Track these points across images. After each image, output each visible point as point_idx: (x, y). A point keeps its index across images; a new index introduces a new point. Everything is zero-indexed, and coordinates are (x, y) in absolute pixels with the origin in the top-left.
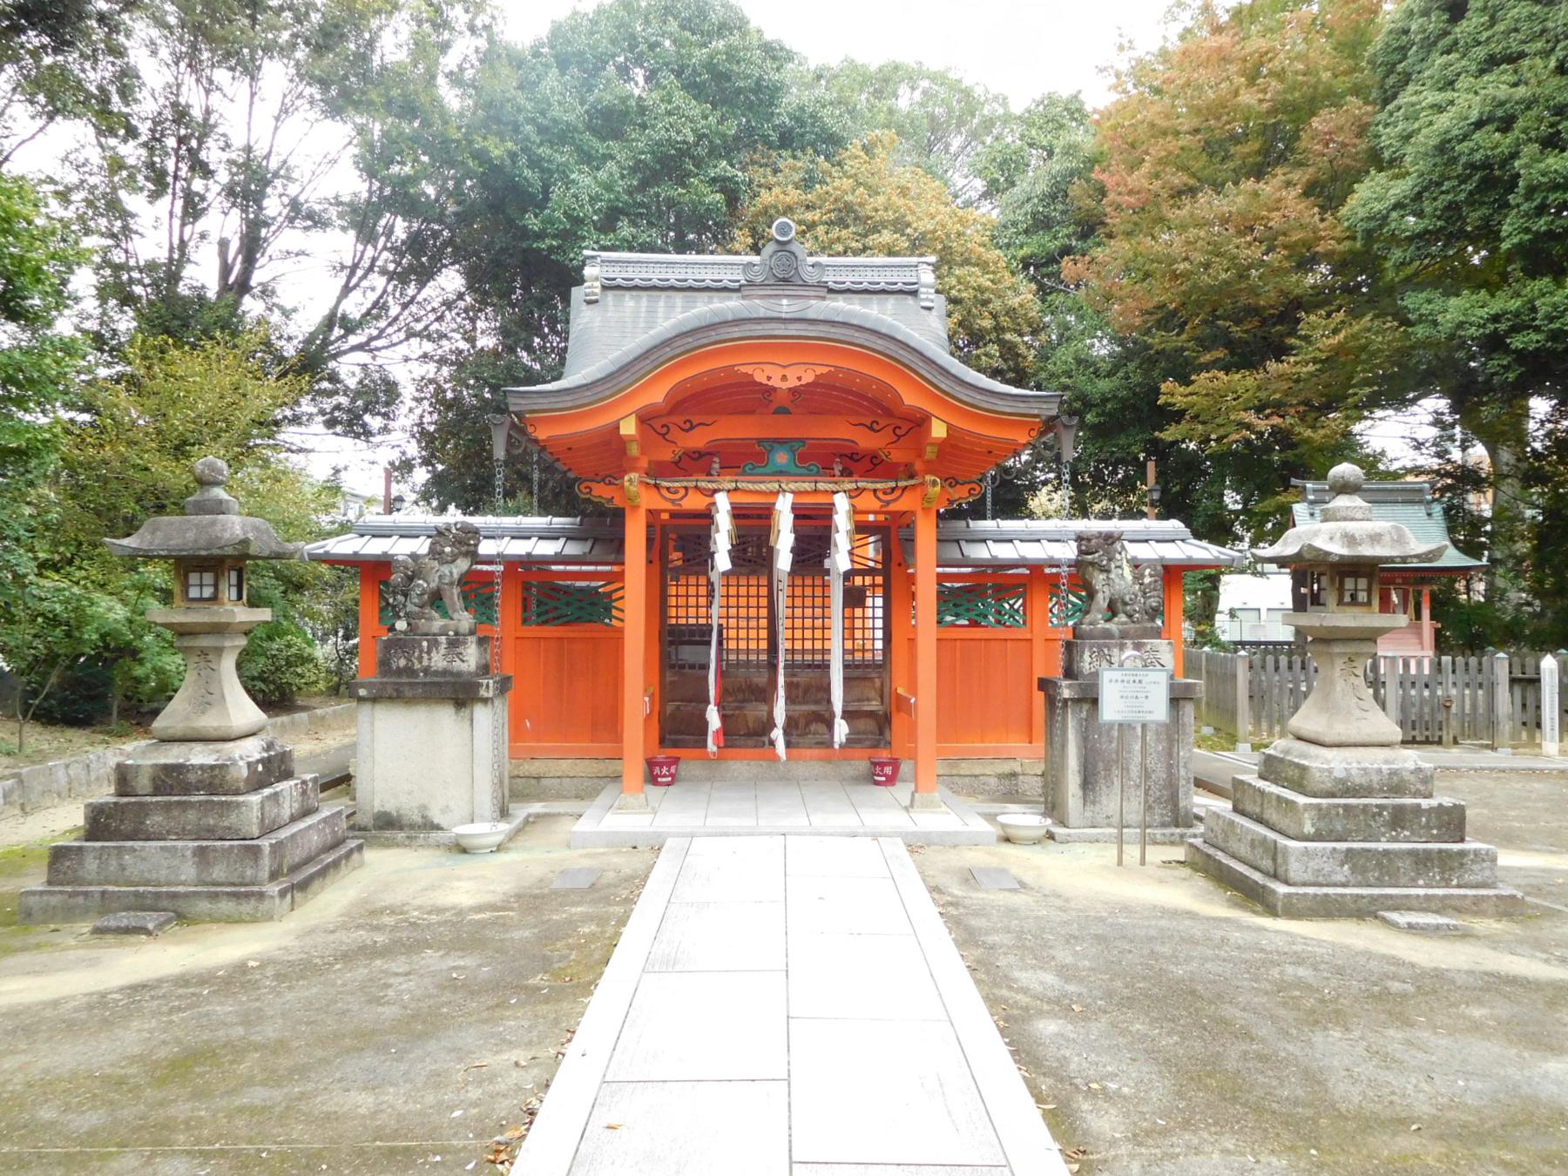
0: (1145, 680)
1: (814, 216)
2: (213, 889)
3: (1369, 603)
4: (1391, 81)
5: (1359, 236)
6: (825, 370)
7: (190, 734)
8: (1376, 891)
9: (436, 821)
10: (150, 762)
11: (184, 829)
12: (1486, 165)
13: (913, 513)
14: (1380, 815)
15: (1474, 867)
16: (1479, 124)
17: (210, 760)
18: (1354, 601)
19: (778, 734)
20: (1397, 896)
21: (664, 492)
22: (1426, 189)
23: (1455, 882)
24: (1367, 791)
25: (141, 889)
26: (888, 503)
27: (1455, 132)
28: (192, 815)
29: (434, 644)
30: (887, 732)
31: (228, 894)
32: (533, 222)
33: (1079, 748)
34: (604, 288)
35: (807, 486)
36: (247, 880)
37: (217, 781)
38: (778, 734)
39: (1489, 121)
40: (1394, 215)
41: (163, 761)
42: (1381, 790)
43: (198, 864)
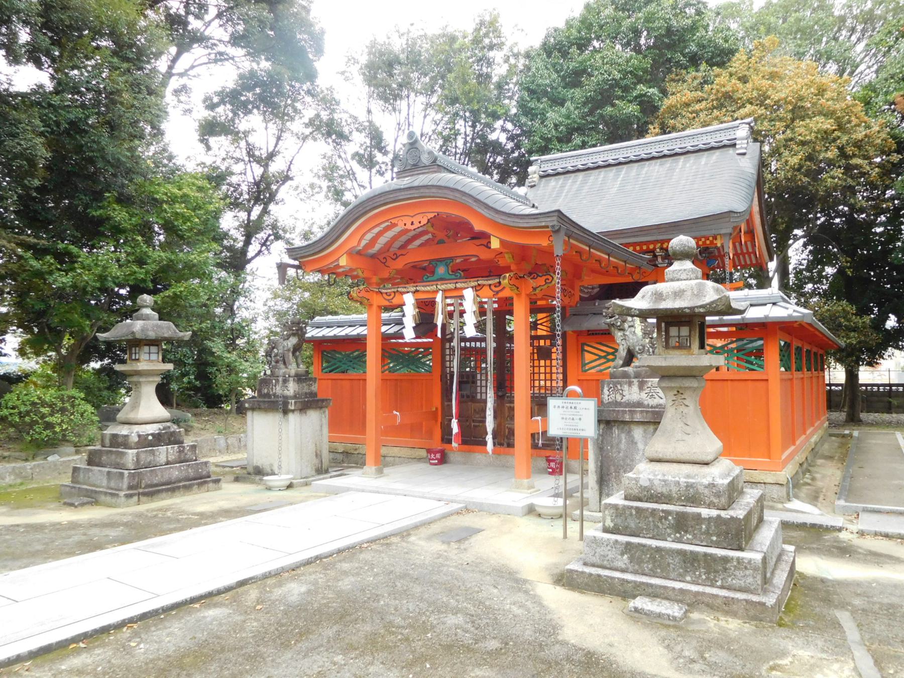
0: (578, 406)
2: (94, 488)
6: (432, 215)
8: (644, 579)
13: (512, 299)
14: (666, 519)
15: (737, 573)
18: (680, 347)
19: (489, 438)
20: (657, 586)
21: (385, 295)
23: (719, 583)
24: (666, 498)
26: (497, 292)
33: (596, 455)
38: (489, 438)
42: (679, 499)
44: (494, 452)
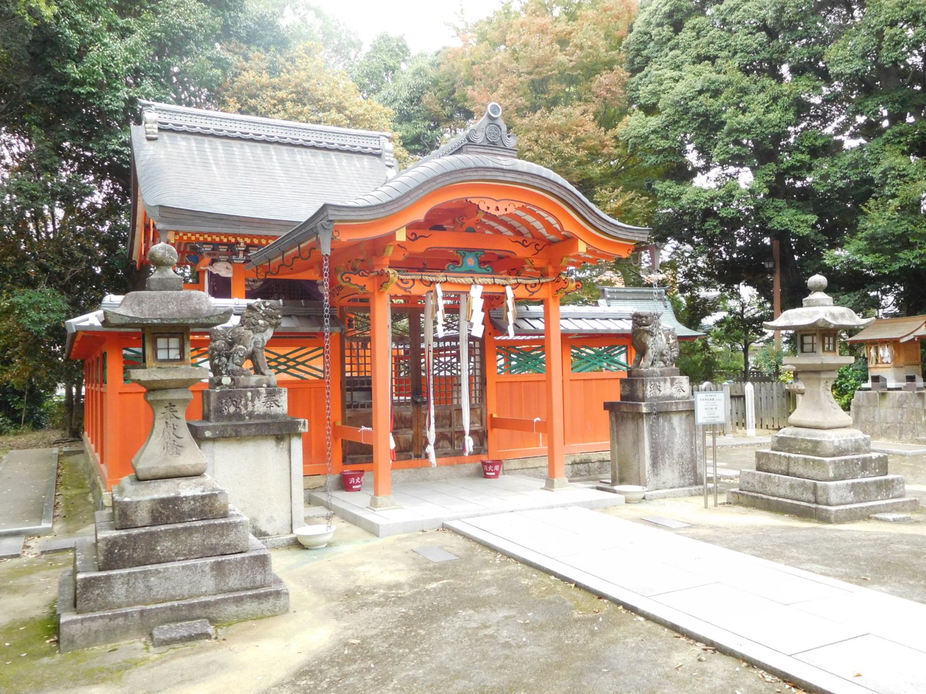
1: (282, 94)
3: (834, 350)
4: (638, 59)
5: (630, 146)
7: (171, 472)
9: (263, 530)
10: (148, 498)
11: (190, 550)
12: (705, 115)
16: (700, 92)
17: (198, 492)
19: (430, 449)
22: (670, 124)
25: (176, 603)
26: (533, 293)
27: (688, 94)
28: (197, 538)
29: (256, 394)
30: (485, 446)
31: (251, 597)
32: (73, 70)
34: (160, 129)
35: (489, 281)
36: (258, 584)
37: (207, 508)
38: (430, 449)
39: (708, 90)
40: (652, 136)
41: (156, 496)
43: (215, 577)
44: (439, 464)
